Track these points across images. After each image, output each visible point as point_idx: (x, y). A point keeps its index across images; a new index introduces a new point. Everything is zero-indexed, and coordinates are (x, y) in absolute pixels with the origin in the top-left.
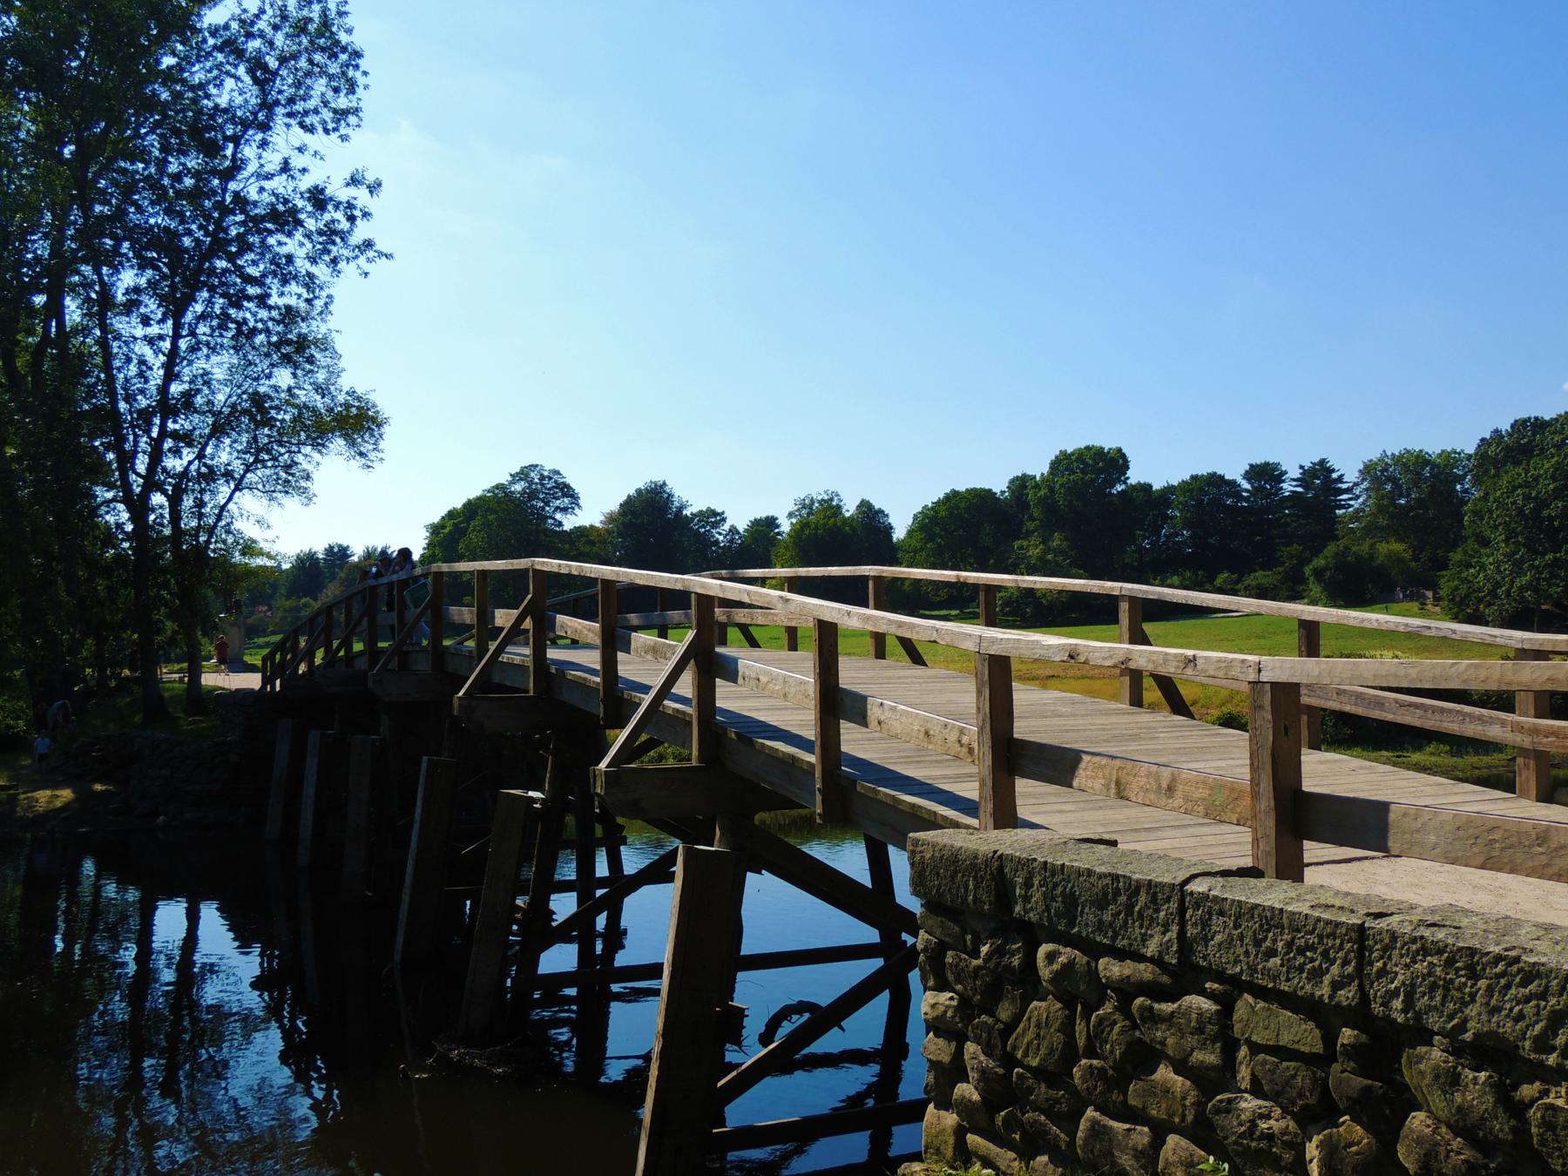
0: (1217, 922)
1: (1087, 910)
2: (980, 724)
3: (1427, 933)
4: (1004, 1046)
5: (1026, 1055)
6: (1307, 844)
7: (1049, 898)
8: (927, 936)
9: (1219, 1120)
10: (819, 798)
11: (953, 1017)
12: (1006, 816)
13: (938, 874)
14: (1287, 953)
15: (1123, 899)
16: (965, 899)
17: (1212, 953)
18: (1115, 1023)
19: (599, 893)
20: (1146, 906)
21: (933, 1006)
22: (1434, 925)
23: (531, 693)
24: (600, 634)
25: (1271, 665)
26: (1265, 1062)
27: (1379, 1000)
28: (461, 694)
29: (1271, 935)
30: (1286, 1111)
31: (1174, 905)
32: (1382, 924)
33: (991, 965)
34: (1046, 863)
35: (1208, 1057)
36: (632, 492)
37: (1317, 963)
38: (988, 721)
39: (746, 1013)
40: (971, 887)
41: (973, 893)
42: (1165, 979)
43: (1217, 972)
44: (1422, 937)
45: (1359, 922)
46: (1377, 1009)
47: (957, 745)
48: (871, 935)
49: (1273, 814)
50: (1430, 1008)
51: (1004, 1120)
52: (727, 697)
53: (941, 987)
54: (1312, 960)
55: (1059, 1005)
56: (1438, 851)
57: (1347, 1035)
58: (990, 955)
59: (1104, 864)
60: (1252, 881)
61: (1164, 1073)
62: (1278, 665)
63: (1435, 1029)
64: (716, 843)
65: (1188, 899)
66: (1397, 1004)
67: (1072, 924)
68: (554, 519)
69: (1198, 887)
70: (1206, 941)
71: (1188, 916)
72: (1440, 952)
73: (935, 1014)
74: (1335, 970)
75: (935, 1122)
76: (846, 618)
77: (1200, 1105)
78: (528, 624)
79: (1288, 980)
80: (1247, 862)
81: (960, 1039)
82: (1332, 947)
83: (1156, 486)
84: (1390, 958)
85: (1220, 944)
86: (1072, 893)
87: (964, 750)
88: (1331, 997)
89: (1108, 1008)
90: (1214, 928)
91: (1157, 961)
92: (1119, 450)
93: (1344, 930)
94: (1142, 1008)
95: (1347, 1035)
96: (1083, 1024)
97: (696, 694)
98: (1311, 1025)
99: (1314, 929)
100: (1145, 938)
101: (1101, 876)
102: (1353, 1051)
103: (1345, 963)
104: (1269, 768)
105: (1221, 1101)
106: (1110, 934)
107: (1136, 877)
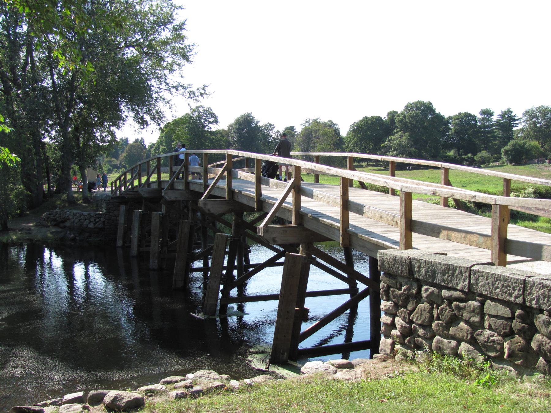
0: (481, 279)
1: (439, 275)
2: (401, 214)
3: (544, 282)
4: (409, 316)
5: (417, 320)
6: (508, 255)
7: (427, 271)
8: (383, 284)
9: (478, 338)
10: (341, 238)
11: (392, 309)
12: (408, 245)
13: (388, 264)
14: (502, 288)
15: (451, 272)
16: (397, 272)
17: (479, 289)
18: (446, 310)
19: (251, 269)
20: (458, 274)
21: (385, 306)
22: (546, 279)
23: (227, 199)
24: (255, 178)
25: (499, 199)
26: (492, 321)
27: (529, 301)
28: (202, 198)
29: (497, 282)
30: (499, 335)
31: (467, 274)
32: (531, 279)
33: (406, 293)
34: (426, 260)
35: (476, 319)
36: (239, 116)
37: (511, 291)
38: (404, 214)
39: (309, 311)
40: (400, 268)
41: (400, 269)
42: (463, 296)
43: (480, 294)
44: (542, 283)
45: (524, 278)
46: (528, 304)
47: (392, 221)
48: (346, 286)
49: (498, 246)
50: (543, 303)
51: (408, 341)
52: (306, 203)
53: (388, 300)
54: (509, 290)
55: (428, 305)
56: (548, 258)
57: (518, 312)
58: (405, 290)
59: (445, 261)
60: (491, 267)
61: (462, 324)
62: (502, 199)
63: (545, 309)
64: (300, 253)
65: (472, 272)
66: (534, 302)
67: (434, 279)
68: (208, 126)
69: (475, 268)
70: (477, 284)
71: (472, 277)
72: (547, 287)
73: (386, 308)
74: (516, 293)
75: (384, 342)
76: (352, 177)
77: (472, 334)
78: (226, 174)
79: (502, 296)
80: (489, 261)
81: (394, 316)
82: (516, 286)
83: (446, 117)
84: (533, 289)
85: (481, 286)
86: (434, 270)
87: (394, 223)
88: (515, 301)
89: (444, 306)
90: (480, 280)
91: (462, 291)
92: (430, 102)
93: (519, 281)
94: (456, 305)
95: (518, 312)
96: (436, 310)
97: (294, 201)
98: (508, 309)
99: (511, 280)
100: (457, 284)
101: (444, 265)
102: (520, 316)
103: (519, 290)
104: (497, 232)
105: (479, 332)
106: (446, 282)
107: (455, 265)
